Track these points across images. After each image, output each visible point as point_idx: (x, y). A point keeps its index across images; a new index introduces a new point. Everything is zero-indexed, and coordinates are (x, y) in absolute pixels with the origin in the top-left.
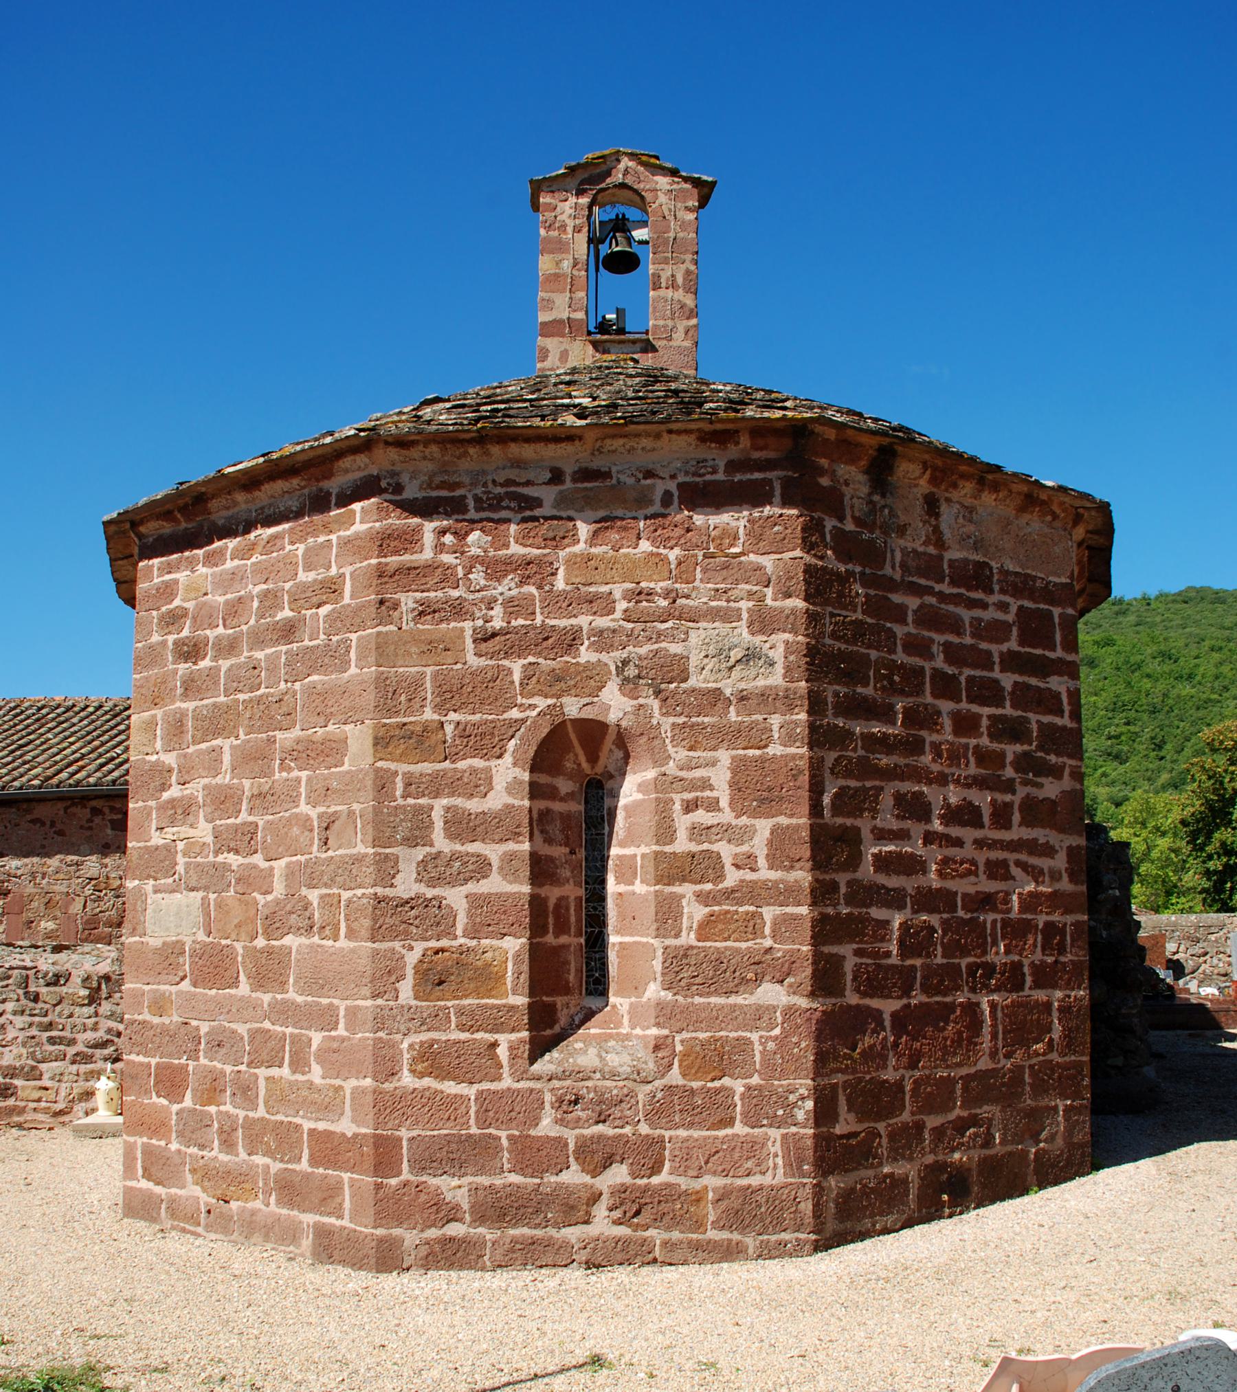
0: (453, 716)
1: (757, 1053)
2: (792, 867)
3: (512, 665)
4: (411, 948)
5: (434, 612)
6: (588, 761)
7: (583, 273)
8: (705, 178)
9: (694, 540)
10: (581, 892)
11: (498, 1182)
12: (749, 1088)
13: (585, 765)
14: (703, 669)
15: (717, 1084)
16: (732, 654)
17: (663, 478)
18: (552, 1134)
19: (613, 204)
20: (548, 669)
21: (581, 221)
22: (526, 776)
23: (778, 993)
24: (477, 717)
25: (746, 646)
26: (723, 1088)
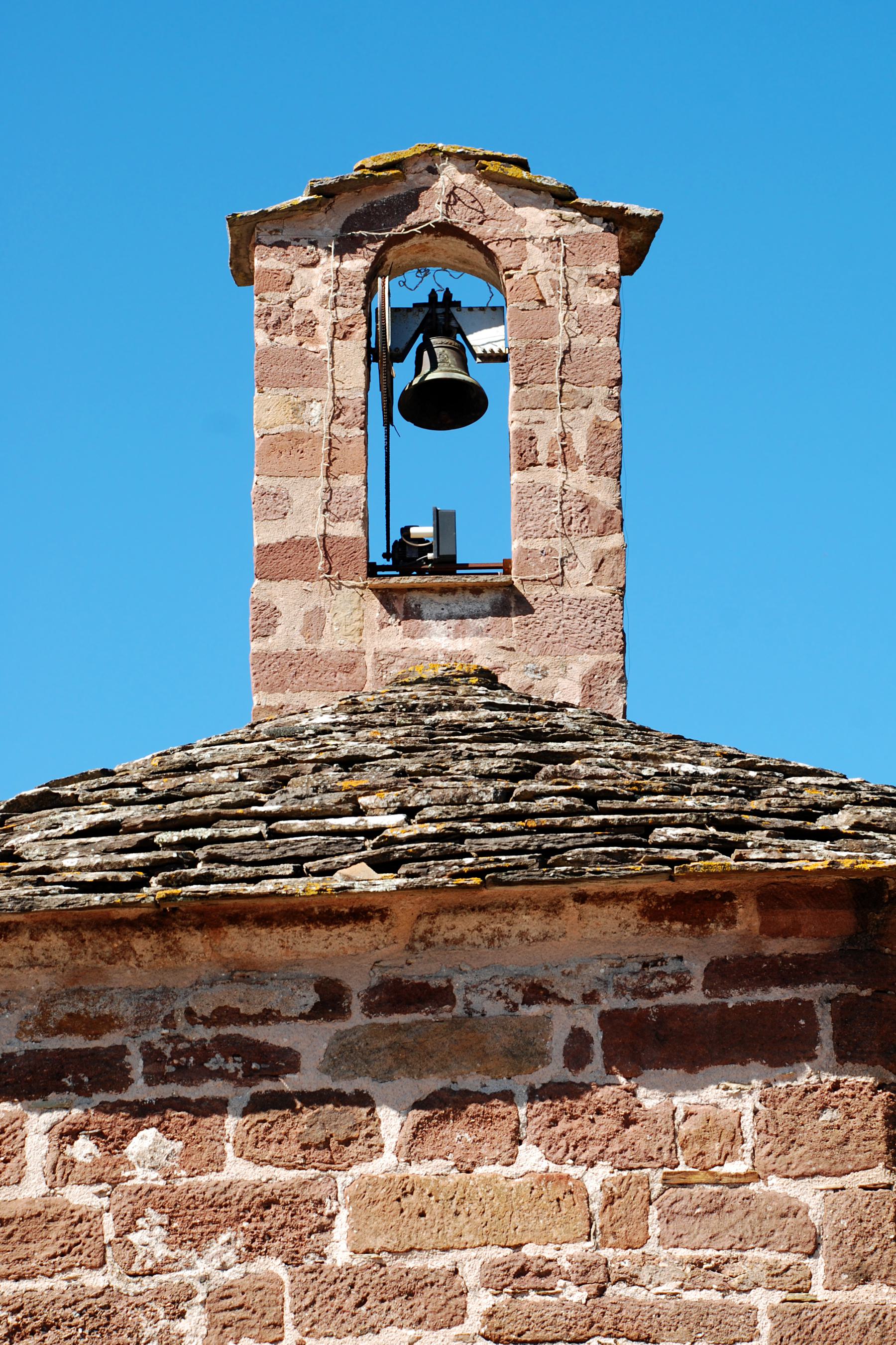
5: (45, 1327)
7: (357, 431)
8: (634, 209)
9: (642, 1145)
17: (568, 1002)
19: (423, 268)
21: (351, 311)
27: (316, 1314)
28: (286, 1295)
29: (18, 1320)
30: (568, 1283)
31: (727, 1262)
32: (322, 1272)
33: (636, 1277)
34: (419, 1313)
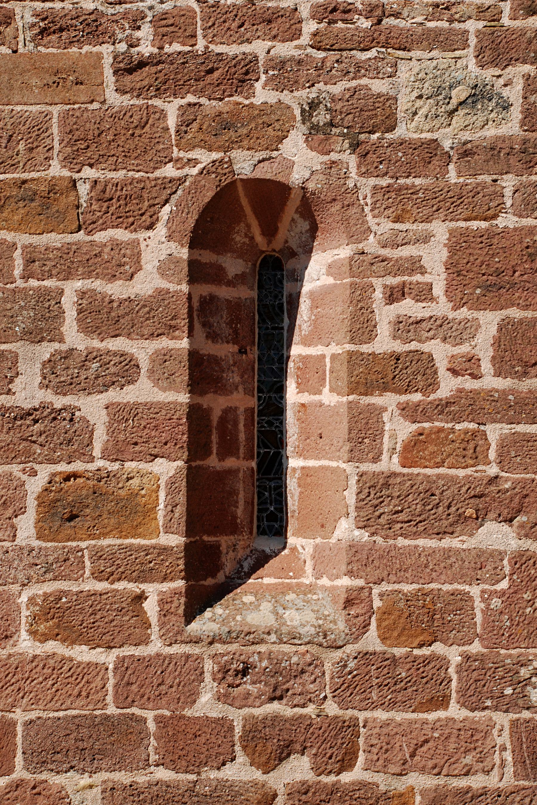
0: (88, 172)
1: (478, 612)
2: (525, 374)
3: (166, 107)
4: (34, 473)
5: (61, 30)
6: (264, 233)
10: (253, 402)
11: (141, 779)
12: (467, 657)
13: (259, 239)
14: (415, 113)
15: (426, 651)
16: (454, 93)
18: (214, 714)
20: (213, 112)
22: (184, 253)
23: (505, 535)
24: (120, 174)
25: (472, 82)
26: (434, 657)
27: (215, 31)
28: (198, 19)
29: (45, 24)
30: (361, 17)
31: (454, 4)
32: (218, 7)
33: (400, 13)
34: (274, 33)
